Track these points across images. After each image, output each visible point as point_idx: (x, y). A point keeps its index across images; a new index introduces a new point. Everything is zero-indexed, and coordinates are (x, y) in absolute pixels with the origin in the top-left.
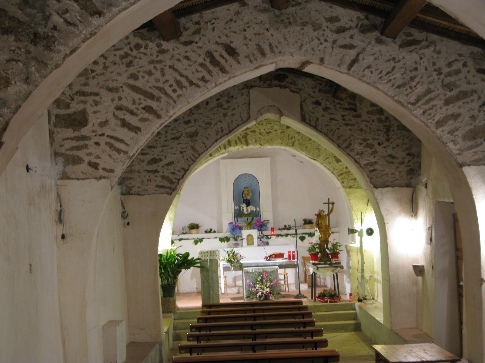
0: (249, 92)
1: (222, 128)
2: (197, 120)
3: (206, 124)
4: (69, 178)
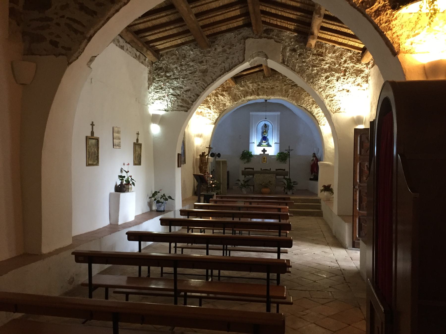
0: (245, 42)
1: (224, 67)
2: (208, 61)
3: (214, 64)
4: (33, 54)
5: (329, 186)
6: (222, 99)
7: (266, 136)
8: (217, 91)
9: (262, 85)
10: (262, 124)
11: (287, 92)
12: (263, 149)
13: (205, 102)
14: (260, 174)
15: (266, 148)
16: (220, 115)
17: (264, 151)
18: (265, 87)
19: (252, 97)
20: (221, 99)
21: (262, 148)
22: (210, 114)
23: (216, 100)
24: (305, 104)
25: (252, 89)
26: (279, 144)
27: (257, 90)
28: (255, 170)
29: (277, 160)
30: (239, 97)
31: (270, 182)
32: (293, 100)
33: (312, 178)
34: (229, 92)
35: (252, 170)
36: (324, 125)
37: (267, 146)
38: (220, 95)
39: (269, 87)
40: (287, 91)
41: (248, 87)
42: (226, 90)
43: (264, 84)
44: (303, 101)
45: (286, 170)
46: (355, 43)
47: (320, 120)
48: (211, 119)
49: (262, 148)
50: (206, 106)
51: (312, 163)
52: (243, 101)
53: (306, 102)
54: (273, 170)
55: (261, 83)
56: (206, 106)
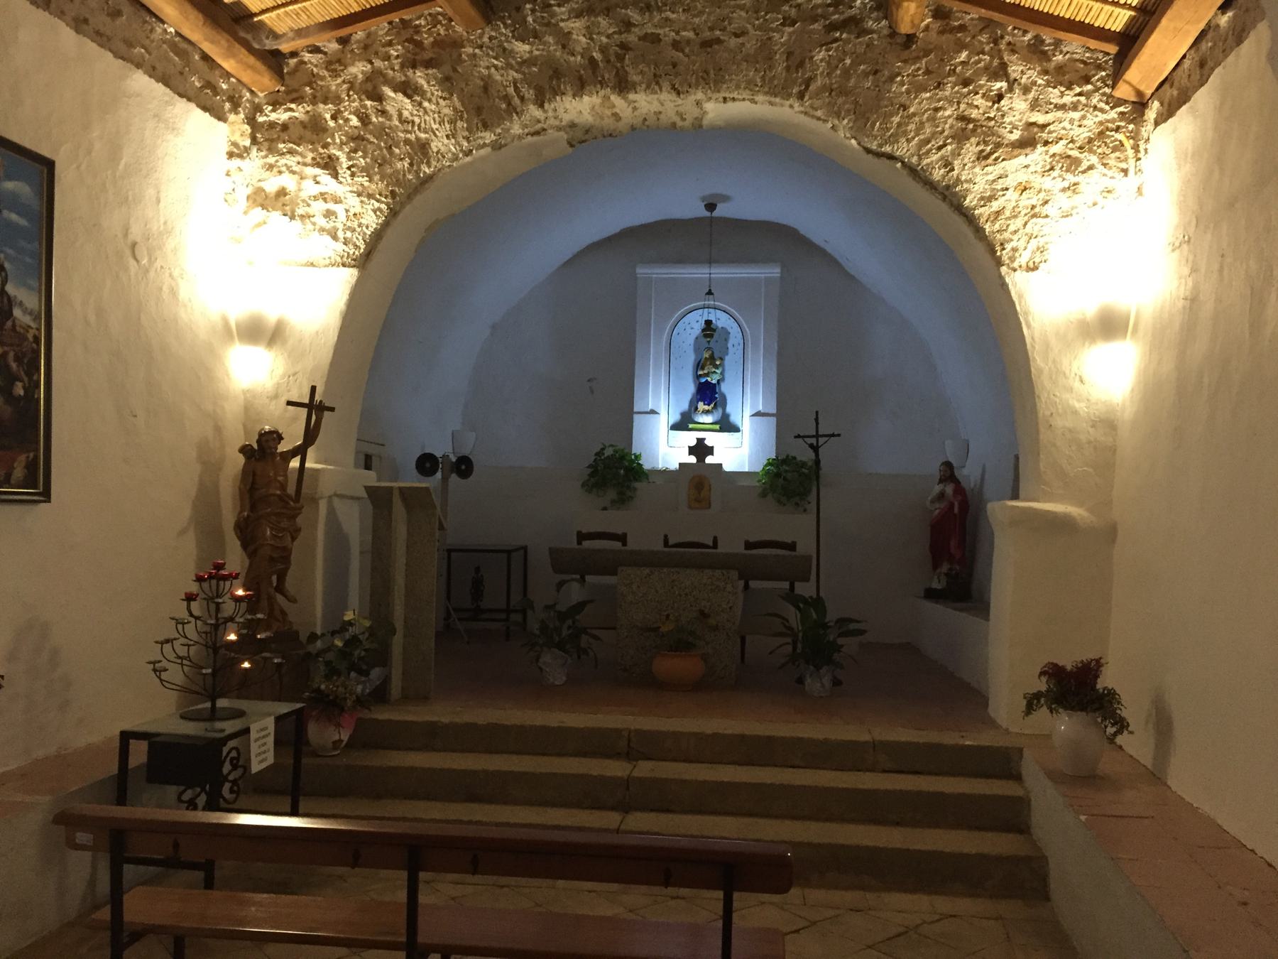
5: (1089, 671)
6: (406, 114)
7: (713, 379)
8: (378, 63)
9: (645, 23)
10: (693, 325)
11: (801, 65)
12: (693, 443)
13: (308, 134)
14: (647, 571)
15: (711, 439)
16: (393, 213)
17: (701, 450)
18: (668, 34)
19: (586, 98)
20: (400, 115)
21: (690, 438)
22: (331, 206)
23: (367, 116)
24: (908, 141)
25: (587, 49)
26: (773, 420)
27: (613, 59)
28: (632, 545)
29: (764, 495)
30: (507, 99)
31: (703, 615)
32: (838, 115)
33: (936, 585)
34: (447, 68)
35: (617, 545)
36: (1035, 268)
37: (717, 427)
38: (395, 91)
39: (690, 34)
40: (797, 61)
41: (565, 40)
42: (431, 59)
43: (657, 17)
44: (896, 119)
45: (801, 549)
46: (1113, 8)
47: (1006, 235)
48: (340, 234)
49: (690, 438)
50: (310, 155)
51: (937, 511)
52: (537, 133)
53: (921, 125)
54: (732, 545)
55: (642, 12)
56: (310, 155)
